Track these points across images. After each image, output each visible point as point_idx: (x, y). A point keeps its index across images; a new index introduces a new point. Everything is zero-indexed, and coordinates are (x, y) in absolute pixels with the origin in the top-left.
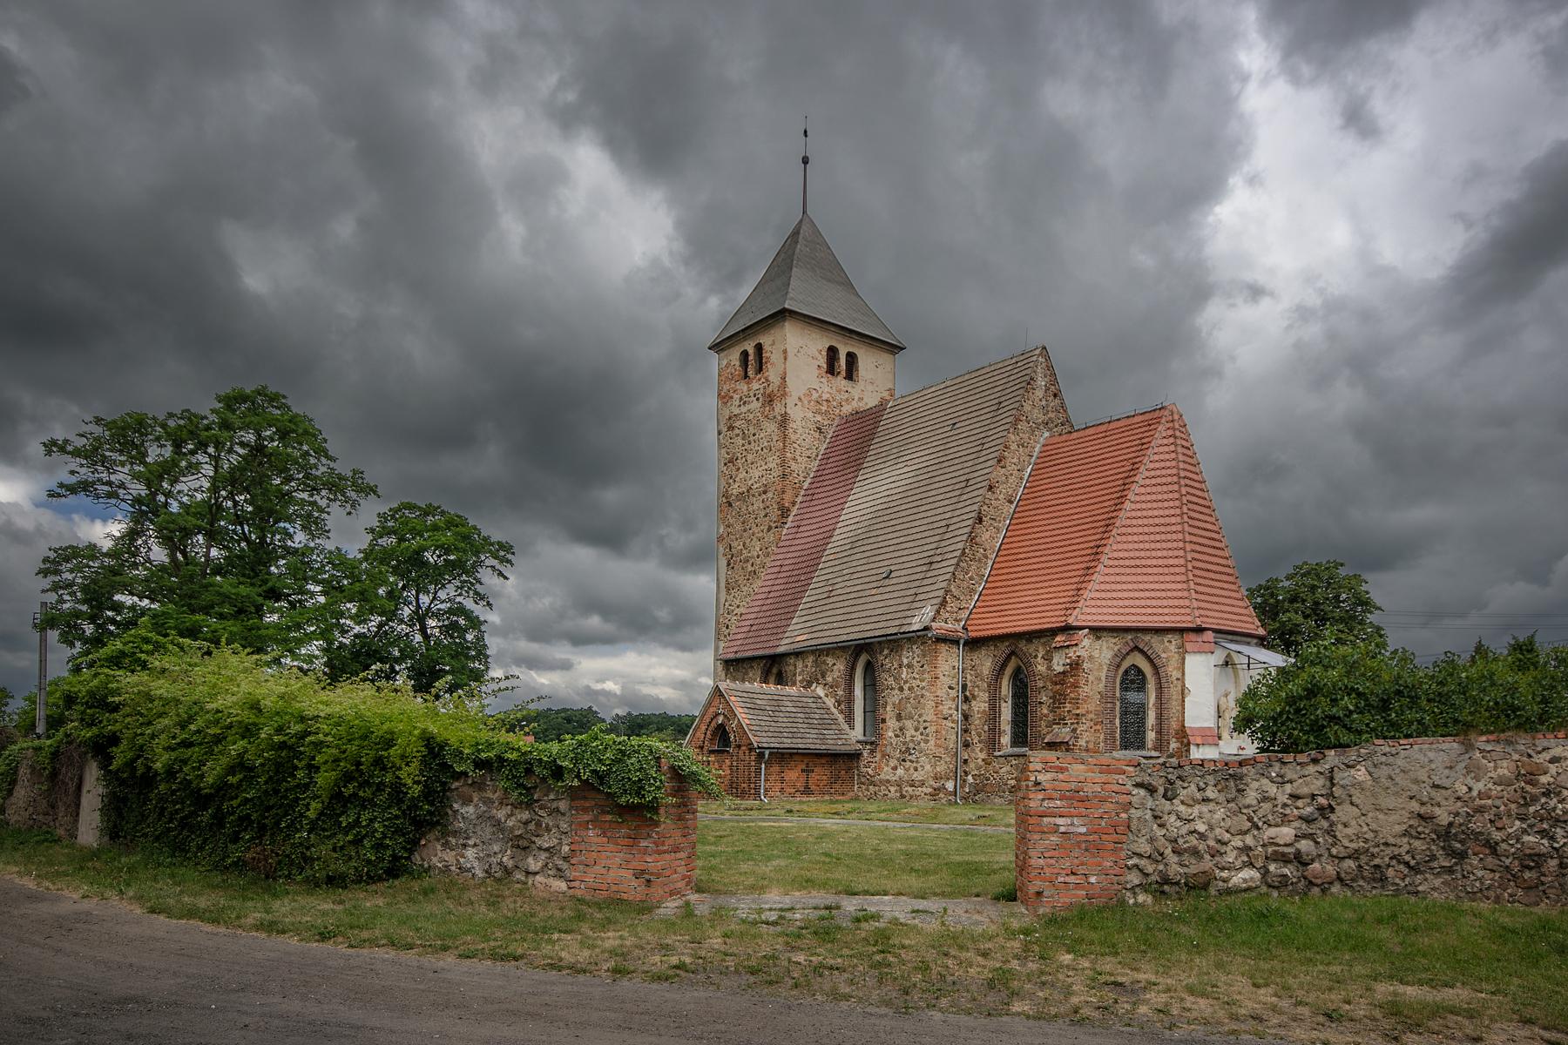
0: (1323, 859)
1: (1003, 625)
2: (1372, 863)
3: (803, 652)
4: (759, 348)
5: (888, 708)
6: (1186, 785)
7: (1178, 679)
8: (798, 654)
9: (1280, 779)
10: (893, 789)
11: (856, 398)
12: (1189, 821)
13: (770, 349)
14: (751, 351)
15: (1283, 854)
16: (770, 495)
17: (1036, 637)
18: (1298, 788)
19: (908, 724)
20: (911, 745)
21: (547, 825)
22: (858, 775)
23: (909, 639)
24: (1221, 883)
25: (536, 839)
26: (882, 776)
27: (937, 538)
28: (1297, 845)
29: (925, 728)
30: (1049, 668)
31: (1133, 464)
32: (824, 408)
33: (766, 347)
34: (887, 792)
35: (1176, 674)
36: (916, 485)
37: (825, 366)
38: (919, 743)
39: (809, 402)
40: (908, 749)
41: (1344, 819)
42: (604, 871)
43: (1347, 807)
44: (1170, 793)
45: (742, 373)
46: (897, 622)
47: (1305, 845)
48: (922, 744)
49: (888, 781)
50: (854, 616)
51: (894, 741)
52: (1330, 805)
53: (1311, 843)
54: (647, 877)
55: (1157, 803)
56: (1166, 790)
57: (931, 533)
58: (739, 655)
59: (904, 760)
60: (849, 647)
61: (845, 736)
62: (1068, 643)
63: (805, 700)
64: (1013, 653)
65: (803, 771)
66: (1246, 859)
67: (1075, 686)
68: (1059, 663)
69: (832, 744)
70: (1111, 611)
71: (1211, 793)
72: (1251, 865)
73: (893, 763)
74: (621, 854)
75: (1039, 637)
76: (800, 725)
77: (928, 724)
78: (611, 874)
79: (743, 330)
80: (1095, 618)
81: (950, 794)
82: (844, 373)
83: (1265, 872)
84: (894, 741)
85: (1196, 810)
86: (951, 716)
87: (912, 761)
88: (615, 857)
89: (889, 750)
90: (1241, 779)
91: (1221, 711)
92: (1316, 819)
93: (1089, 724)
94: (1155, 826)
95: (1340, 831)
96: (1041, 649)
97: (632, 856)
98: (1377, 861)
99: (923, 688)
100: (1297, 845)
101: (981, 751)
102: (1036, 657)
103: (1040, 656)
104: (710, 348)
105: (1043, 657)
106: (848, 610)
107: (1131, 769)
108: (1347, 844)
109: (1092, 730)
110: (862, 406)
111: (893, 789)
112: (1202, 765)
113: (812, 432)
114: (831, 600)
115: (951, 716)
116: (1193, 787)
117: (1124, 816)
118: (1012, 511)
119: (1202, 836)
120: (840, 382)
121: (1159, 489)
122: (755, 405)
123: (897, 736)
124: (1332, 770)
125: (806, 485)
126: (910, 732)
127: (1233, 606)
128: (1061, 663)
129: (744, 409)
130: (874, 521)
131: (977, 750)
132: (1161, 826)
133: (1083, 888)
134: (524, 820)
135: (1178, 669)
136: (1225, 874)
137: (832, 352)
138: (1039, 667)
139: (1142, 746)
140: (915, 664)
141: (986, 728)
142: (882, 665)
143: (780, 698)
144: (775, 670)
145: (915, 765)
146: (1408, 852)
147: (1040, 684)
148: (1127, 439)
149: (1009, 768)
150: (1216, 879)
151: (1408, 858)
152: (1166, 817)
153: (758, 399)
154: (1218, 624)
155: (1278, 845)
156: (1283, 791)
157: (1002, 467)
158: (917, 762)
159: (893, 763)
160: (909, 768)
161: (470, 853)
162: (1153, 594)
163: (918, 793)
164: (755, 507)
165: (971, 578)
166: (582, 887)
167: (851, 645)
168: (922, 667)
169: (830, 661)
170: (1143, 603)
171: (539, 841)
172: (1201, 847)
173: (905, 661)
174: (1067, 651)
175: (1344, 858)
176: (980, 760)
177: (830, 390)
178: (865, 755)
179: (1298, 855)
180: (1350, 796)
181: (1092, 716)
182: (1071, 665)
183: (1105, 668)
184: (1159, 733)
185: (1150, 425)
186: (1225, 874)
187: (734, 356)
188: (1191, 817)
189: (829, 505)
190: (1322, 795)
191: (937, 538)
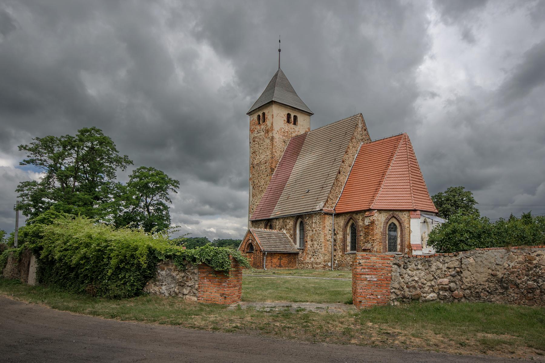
0: (459, 290)
2: (476, 291)
4: (264, 114)
5: (308, 237)
6: (411, 264)
7: (408, 227)
8: (277, 219)
9: (443, 262)
11: (297, 131)
14: (261, 115)
15: (445, 288)
16: (267, 164)
17: (359, 213)
18: (450, 265)
20: (316, 250)
21: (190, 278)
22: (298, 260)
23: (315, 214)
25: (186, 283)
29: (321, 244)
30: (363, 223)
32: (286, 134)
33: (266, 114)
34: (308, 266)
35: (407, 226)
37: (286, 120)
38: (319, 249)
39: (281, 132)
41: (466, 276)
43: (467, 271)
44: (405, 267)
45: (258, 122)
47: (452, 285)
49: (308, 263)
51: (310, 249)
52: (461, 271)
53: (455, 284)
54: (225, 296)
55: (401, 270)
56: (404, 266)
57: (323, 177)
58: (257, 219)
59: (314, 255)
60: (295, 216)
65: (279, 259)
66: (432, 290)
67: (373, 230)
68: (367, 221)
69: (289, 250)
70: (384, 204)
72: (434, 292)
73: (310, 256)
74: (216, 288)
75: (360, 213)
78: (212, 295)
79: (258, 108)
80: (379, 206)
81: (329, 267)
82: (293, 123)
83: (439, 294)
84: (310, 249)
85: (414, 273)
86: (330, 240)
87: (316, 256)
92: (456, 276)
93: (377, 243)
94: (400, 278)
95: (464, 280)
96: (361, 217)
98: (477, 290)
99: (320, 230)
101: (340, 252)
102: (359, 220)
103: (360, 219)
104: (247, 114)
105: (361, 220)
107: (392, 258)
108: (467, 285)
109: (378, 245)
110: (299, 134)
112: (416, 257)
113: (282, 143)
115: (330, 240)
116: (413, 265)
117: (390, 274)
118: (350, 170)
119: (417, 282)
120: (292, 125)
122: (262, 133)
123: (311, 247)
125: (280, 161)
126: (316, 246)
129: (259, 135)
131: (339, 252)
133: (376, 300)
135: (408, 224)
136: (425, 295)
137: (289, 116)
138: (360, 223)
139: (395, 250)
141: (342, 244)
143: (271, 234)
144: (269, 224)
146: (488, 287)
147: (360, 229)
151: (488, 289)
152: (404, 275)
153: (263, 131)
154: (421, 208)
155: (443, 285)
156: (445, 266)
157: (347, 155)
158: (318, 256)
159: (310, 256)
160: (315, 258)
161: (164, 288)
163: (318, 267)
164: (262, 168)
165: (336, 193)
167: (295, 216)
169: (288, 221)
171: (187, 283)
173: (314, 221)
174: (370, 218)
175: (466, 289)
176: (340, 255)
178: (300, 253)
180: (468, 268)
182: (371, 222)
183: (383, 223)
186: (425, 295)
187: (255, 117)
190: (458, 268)
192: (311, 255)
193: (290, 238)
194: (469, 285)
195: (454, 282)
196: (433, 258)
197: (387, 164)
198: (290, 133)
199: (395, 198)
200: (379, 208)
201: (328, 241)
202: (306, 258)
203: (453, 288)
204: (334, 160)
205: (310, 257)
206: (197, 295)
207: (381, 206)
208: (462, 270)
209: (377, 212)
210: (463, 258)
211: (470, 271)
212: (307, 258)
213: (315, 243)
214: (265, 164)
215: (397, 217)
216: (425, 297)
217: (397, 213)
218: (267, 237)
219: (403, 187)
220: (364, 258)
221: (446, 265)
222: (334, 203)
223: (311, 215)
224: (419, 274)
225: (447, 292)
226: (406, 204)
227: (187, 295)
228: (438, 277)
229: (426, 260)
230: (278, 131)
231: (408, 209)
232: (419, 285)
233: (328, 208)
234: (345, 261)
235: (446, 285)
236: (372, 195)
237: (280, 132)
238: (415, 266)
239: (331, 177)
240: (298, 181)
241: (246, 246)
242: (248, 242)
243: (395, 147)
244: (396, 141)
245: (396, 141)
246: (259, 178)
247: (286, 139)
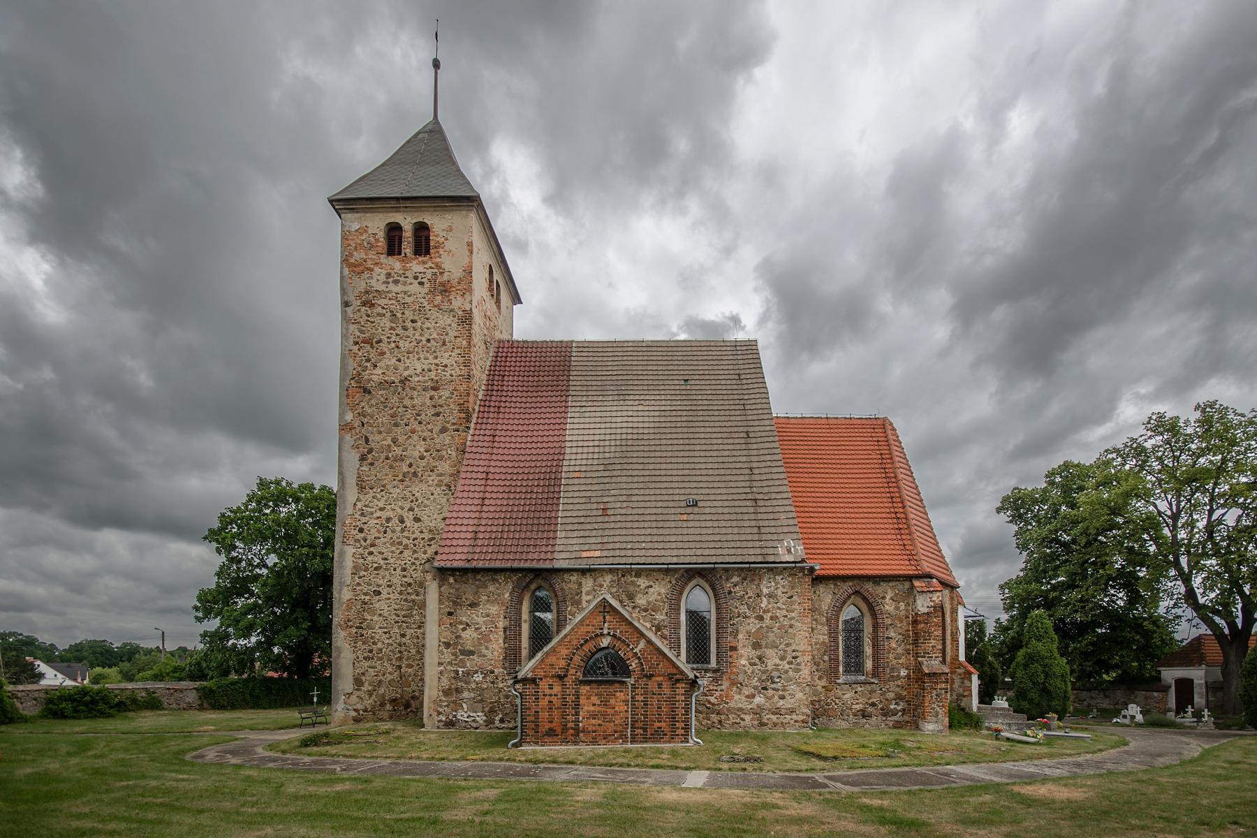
1: (851, 567)
3: (595, 570)
5: (740, 636)
10: (747, 718)
19: (770, 652)
20: (775, 674)
23: (771, 569)
26: (732, 704)
38: (786, 672)
40: (772, 678)
48: (791, 673)
49: (741, 709)
58: (474, 564)
59: (765, 689)
60: (676, 570)
77: (798, 654)
79: (397, 199)
84: (749, 669)
96: (889, 591)
101: (820, 678)
102: (884, 598)
105: (891, 599)
111: (747, 718)
128: (925, 605)
138: (887, 607)
140: (779, 592)
141: (826, 658)
142: (730, 593)
147: (888, 621)
149: (852, 694)
163: (785, 721)
167: (680, 569)
168: (791, 597)
173: (765, 591)
174: (930, 595)
182: (935, 607)
187: (377, 224)
213: (770, 652)
214: (433, 393)
223: (750, 571)
241: (577, 658)
246: (399, 430)
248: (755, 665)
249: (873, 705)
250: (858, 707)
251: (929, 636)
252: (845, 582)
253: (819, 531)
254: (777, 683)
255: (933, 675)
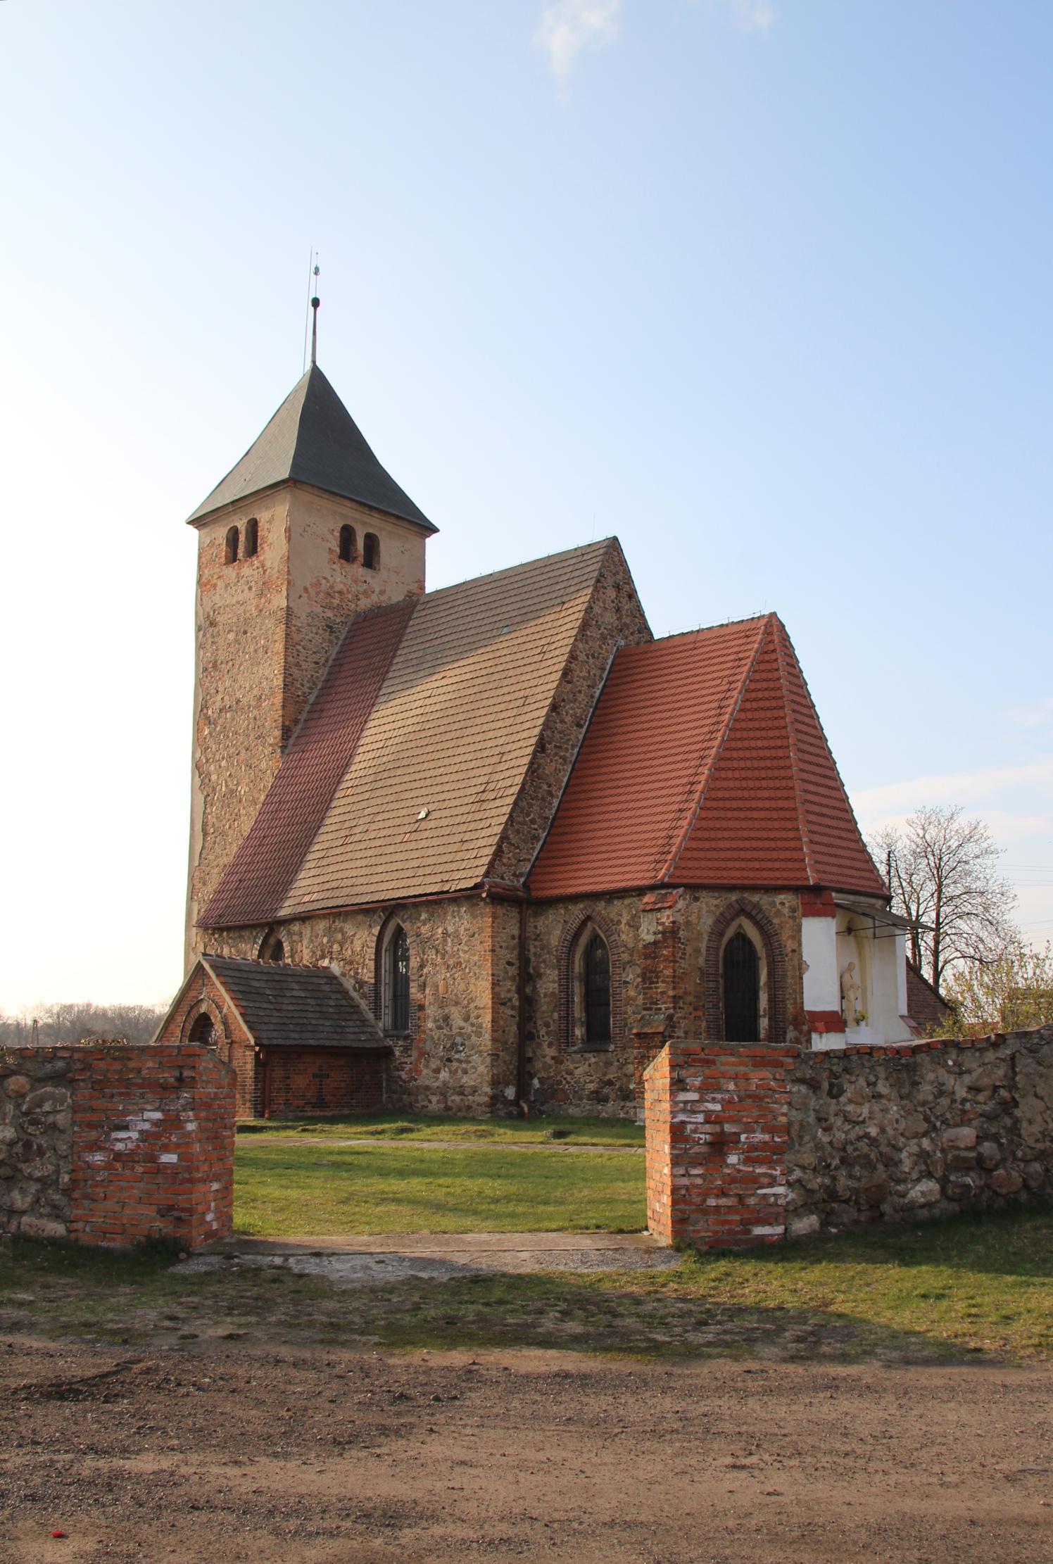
0: (1008, 1164)
4: (253, 525)
6: (853, 1079)
7: (793, 951)
8: (304, 918)
9: (956, 1069)
10: (434, 1099)
11: (377, 590)
12: (858, 1123)
13: (267, 526)
15: (965, 1160)
17: (619, 898)
18: (977, 1079)
20: (458, 1040)
21: (40, 1147)
22: (388, 1080)
24: (896, 1199)
25: (23, 1166)
27: (489, 770)
28: (980, 1149)
30: (637, 938)
31: (730, 683)
32: (336, 602)
33: (263, 525)
34: (425, 1103)
35: (790, 945)
36: (458, 702)
37: (338, 550)
38: (469, 1037)
39: (318, 593)
40: (454, 1045)
41: (1028, 1115)
42: (117, 1208)
43: (1031, 1100)
44: (835, 1090)
46: (438, 878)
47: (988, 1148)
48: (474, 1038)
50: (380, 869)
52: (1013, 1099)
53: (995, 1146)
54: (176, 1214)
55: (821, 1101)
56: (831, 1086)
57: (480, 763)
58: (295, 1038)
59: (449, 1060)
61: (369, 1030)
62: (659, 905)
63: (316, 980)
64: (588, 918)
65: (315, 1076)
66: (923, 1167)
69: (353, 1039)
70: (710, 864)
71: (882, 1088)
72: (929, 1175)
73: (434, 1064)
74: (141, 1185)
75: (622, 898)
76: (311, 1015)
78: (127, 1211)
79: (233, 502)
80: (691, 873)
81: (511, 1103)
82: (361, 560)
83: (944, 1182)
85: (865, 1110)
86: (510, 1000)
87: (459, 1061)
88: (132, 1188)
89: (428, 1046)
90: (915, 1070)
91: (845, 992)
92: (998, 1116)
94: (820, 1132)
95: (1025, 1129)
97: (155, 1187)
100: (980, 1149)
101: (550, 1045)
102: (619, 922)
103: (624, 921)
104: (189, 523)
105: (628, 924)
106: (373, 861)
107: (790, 1060)
108: (1033, 1145)
109: (692, 1017)
110: (385, 600)
111: (434, 1099)
112: (870, 1054)
113: (321, 632)
114: (349, 848)
115: (510, 1000)
116: (862, 1082)
118: (581, 737)
119: (873, 1142)
120: (358, 570)
121: (762, 714)
123: (440, 1028)
124: (1013, 1057)
125: (312, 699)
127: (853, 859)
130: (404, 746)
131: (545, 1045)
132: (827, 1130)
133: (737, 1212)
134: (8, 1140)
136: (901, 1188)
137: (347, 534)
138: (624, 937)
139: (753, 1035)
141: (556, 1016)
143: (284, 978)
145: (464, 1066)
147: (626, 957)
148: (720, 653)
150: (890, 1192)
152: (832, 1120)
153: (250, 588)
154: (838, 882)
155: (958, 1149)
156: (962, 1083)
157: (569, 682)
158: (468, 1062)
159: (434, 1064)
160: (456, 1071)
162: (761, 844)
165: (533, 822)
166: (88, 1229)
169: (349, 928)
170: (749, 854)
171: (27, 1169)
172: (873, 1156)
174: (659, 915)
175: (1030, 1161)
176: (548, 1058)
177: (344, 581)
178: (397, 1053)
179: (980, 1160)
180: (1034, 1086)
181: (690, 999)
182: (663, 933)
183: (706, 937)
184: (772, 1019)
185: (747, 637)
186: (901, 1188)
188: (861, 1119)
189: (708, 854)
190: (1004, 1087)
191: (489, 770)
192: (441, 1060)
193: (353, 994)
194: (1040, 1146)
195: (995, 1138)
196: (923, 1055)
197: (715, 720)
198: (350, 596)
199: (747, 844)
200: (692, 881)
201: (504, 1004)
202: (418, 1072)
203: (991, 1160)
204: (520, 702)
205: (434, 1066)
206: (67, 1211)
207: (698, 873)
208: (1017, 1096)
209: (684, 892)
210: (1017, 1054)
211: (1042, 1099)
212: (425, 1072)
215: (754, 913)
216: (903, 1195)
217: (755, 898)
218: (268, 992)
219: (773, 804)
220: (694, 1061)
221: (967, 1079)
222: (525, 860)
224: (879, 1115)
225: (972, 1174)
226: (783, 865)
227: (23, 1213)
228: (943, 1122)
229: (903, 1064)
230: (306, 590)
231: (792, 883)
232: (881, 1153)
233: (502, 878)
234: (569, 1077)
235: (968, 1149)
236: (664, 834)
237: (313, 593)
238: (869, 1085)
239: (513, 763)
240: (386, 774)
242: (195, 1010)
243: (740, 659)
244: (741, 641)
245: (741, 641)
247: (338, 621)
248: (442, 1028)
249: (610, 1083)
250: (592, 1086)
251: (657, 977)
252: (576, 903)
253: (745, 834)
254: (461, 1052)
255: (870, 1113)
